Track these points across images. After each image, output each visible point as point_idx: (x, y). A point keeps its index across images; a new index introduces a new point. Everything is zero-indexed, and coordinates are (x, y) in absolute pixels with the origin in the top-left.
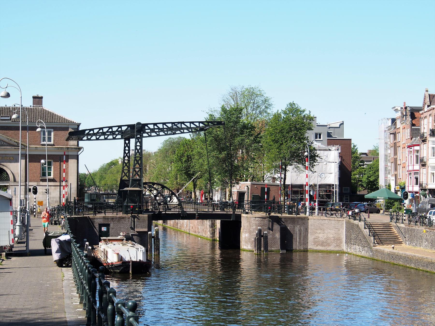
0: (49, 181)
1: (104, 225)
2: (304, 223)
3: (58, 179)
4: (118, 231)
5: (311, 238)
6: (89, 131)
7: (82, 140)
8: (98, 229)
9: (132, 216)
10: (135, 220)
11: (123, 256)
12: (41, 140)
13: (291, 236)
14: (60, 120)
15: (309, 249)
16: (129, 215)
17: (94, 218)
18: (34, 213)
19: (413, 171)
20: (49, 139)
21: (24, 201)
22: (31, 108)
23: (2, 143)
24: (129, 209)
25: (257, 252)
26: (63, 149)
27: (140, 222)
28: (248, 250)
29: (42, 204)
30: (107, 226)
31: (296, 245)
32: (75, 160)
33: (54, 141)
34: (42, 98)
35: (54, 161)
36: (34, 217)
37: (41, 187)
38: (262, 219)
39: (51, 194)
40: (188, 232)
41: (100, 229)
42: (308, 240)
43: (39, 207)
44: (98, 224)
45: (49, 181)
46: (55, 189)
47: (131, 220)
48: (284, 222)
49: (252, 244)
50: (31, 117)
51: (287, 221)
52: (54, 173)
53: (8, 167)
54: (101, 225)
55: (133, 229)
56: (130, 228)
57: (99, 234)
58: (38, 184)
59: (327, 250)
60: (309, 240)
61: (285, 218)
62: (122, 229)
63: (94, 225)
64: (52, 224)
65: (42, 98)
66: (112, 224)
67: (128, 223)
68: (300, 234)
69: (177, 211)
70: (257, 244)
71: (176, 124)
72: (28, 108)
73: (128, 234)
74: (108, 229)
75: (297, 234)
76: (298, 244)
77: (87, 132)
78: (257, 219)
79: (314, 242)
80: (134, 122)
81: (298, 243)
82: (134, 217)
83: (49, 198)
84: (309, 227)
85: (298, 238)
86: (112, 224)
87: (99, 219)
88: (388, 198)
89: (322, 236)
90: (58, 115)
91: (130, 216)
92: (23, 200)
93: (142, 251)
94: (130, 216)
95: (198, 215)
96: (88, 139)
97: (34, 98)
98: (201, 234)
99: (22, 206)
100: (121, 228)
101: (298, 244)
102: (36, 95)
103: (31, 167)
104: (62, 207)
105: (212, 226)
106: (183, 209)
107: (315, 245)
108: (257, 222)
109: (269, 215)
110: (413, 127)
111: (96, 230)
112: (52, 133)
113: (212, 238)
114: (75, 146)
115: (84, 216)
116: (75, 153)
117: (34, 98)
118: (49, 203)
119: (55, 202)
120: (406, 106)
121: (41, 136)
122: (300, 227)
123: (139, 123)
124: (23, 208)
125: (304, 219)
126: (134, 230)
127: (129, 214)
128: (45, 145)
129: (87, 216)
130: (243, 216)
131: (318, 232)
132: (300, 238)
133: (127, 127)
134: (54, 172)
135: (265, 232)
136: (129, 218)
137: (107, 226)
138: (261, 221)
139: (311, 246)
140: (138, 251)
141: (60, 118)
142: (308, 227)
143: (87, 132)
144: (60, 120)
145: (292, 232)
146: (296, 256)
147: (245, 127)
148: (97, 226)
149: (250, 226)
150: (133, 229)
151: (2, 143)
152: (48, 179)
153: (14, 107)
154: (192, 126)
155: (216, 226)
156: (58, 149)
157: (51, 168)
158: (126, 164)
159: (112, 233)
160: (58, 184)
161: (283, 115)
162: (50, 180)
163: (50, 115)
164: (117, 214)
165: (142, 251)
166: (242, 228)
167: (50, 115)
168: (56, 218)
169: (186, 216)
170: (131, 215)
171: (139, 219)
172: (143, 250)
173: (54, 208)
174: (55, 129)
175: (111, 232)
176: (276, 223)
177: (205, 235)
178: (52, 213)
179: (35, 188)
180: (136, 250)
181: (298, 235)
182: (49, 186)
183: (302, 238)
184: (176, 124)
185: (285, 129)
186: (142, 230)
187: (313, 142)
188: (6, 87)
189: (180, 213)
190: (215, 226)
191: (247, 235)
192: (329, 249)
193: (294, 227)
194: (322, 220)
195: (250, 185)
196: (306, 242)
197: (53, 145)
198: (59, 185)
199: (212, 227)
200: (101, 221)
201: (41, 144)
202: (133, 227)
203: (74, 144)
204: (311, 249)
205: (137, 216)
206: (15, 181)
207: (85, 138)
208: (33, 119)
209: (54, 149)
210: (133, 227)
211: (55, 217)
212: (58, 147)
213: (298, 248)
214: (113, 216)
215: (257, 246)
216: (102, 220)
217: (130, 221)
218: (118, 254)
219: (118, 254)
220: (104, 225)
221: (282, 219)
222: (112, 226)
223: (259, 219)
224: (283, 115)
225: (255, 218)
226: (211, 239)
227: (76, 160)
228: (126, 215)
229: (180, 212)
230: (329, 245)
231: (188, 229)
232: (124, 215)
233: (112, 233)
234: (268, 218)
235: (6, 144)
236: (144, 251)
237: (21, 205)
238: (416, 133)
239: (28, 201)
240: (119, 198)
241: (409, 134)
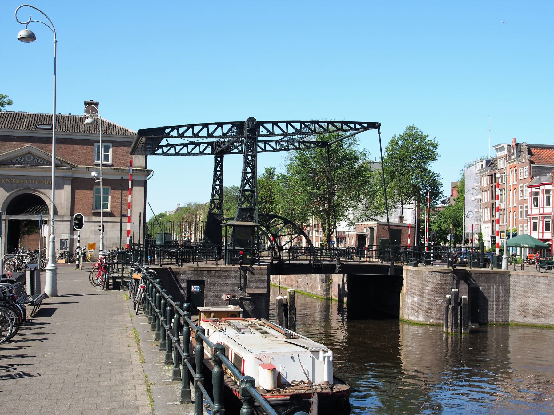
0: (103, 216)
1: (196, 283)
2: (503, 281)
3: (118, 213)
4: (219, 293)
5: (513, 304)
6: (170, 129)
7: (154, 154)
8: (185, 288)
9: (242, 268)
10: (247, 274)
11: (283, 374)
12: (94, 158)
13: (485, 301)
14: (122, 132)
15: (511, 321)
16: (236, 266)
17: (180, 270)
18: (77, 262)
19: (540, 214)
20: (106, 158)
21: (66, 242)
22: (82, 117)
23: (39, 161)
24: (236, 256)
25: (452, 331)
26: (125, 171)
27: (255, 278)
28: (418, 322)
29: (94, 248)
30: (201, 283)
31: (493, 317)
32: (141, 187)
33: (113, 160)
34: (97, 104)
35: (112, 189)
36: (76, 267)
37: (94, 223)
38: (442, 274)
39: (108, 233)
40: (278, 285)
41: (189, 289)
42: (509, 307)
43: (90, 251)
44: (185, 281)
45: (103, 216)
46: (113, 227)
47: (241, 274)
48: (475, 279)
49: (426, 314)
50: (81, 127)
51: (479, 278)
52: (112, 205)
53: (47, 195)
54: (190, 283)
55: (242, 289)
56: (238, 287)
57: (187, 297)
58: (89, 219)
59: (543, 325)
60: (510, 307)
61: (476, 273)
62: (225, 290)
63: (178, 283)
64: (108, 288)
65: (97, 104)
66: (209, 281)
67: (234, 280)
68: (498, 298)
69: (306, 260)
70: (452, 316)
71: (307, 124)
72: (78, 117)
73: (235, 297)
74: (202, 289)
75: (493, 298)
76: (494, 314)
77: (167, 131)
78: (434, 274)
79: (519, 311)
80: (243, 118)
81: (494, 313)
82: (245, 270)
83: (103, 236)
84: (511, 287)
85: (494, 304)
86: (209, 281)
87: (187, 272)
88: (536, 245)
89: (532, 302)
90: (119, 126)
91: (239, 268)
92: (65, 240)
93: (326, 359)
94: (239, 268)
95: (339, 267)
96: (165, 154)
97: (86, 103)
98: (303, 289)
99: (64, 250)
100: (223, 287)
101: (494, 314)
102: (89, 100)
103: (79, 195)
104: (125, 252)
105: (326, 280)
106: (317, 257)
107: (522, 316)
108: (435, 280)
109: (453, 269)
110: (532, 165)
111: (183, 290)
112: (111, 150)
113: (326, 296)
114: (141, 167)
115: (163, 266)
116: (141, 178)
117: (86, 103)
118: (103, 244)
119: (113, 245)
120: (517, 143)
121: (94, 153)
122: (498, 287)
123: (251, 119)
124: (65, 253)
125: (504, 275)
126: (244, 291)
127: (238, 264)
128: (99, 165)
129: (168, 267)
130: (407, 270)
131: (527, 295)
132: (497, 305)
133: (231, 126)
134: (112, 202)
135: (463, 297)
136: (236, 271)
137: (201, 283)
138: (441, 277)
139: (514, 317)
140: (316, 359)
141: (121, 129)
142: (509, 287)
143: (167, 131)
144: (122, 132)
145: (486, 295)
146: (493, 334)
147: (346, 157)
148: (184, 285)
149: (423, 286)
150: (242, 289)
151: (39, 161)
152: (103, 213)
153: (58, 115)
154: (332, 128)
155: (332, 279)
156: (119, 172)
157: (108, 197)
158: (217, 191)
159: (209, 296)
160: (118, 219)
161: (400, 143)
162: (106, 214)
163: (107, 126)
164: (217, 264)
165: (326, 359)
166: (404, 289)
167: (107, 126)
168: (115, 271)
169: (321, 268)
170: (241, 265)
171: (253, 274)
172: (329, 357)
173: (113, 253)
174: (115, 144)
175: (206, 294)
176: (463, 281)
177: (312, 291)
178: (109, 264)
179: (79, 217)
180: (312, 355)
181: (494, 300)
182: (103, 222)
183: (500, 305)
184: (307, 124)
185: (407, 157)
186: (258, 290)
187: (439, 175)
188: (28, 23)
189: (312, 263)
190: (329, 280)
191: (416, 299)
192: (546, 323)
193: (489, 287)
194: (534, 276)
195: (376, 225)
196: (506, 312)
197: (112, 166)
198: (119, 221)
199: (326, 282)
200: (191, 276)
201: (94, 163)
202: (242, 285)
203: (140, 165)
204: (514, 321)
205: (251, 269)
206: (56, 213)
207: (160, 151)
208: (83, 130)
209: (112, 171)
210: (242, 285)
211: (113, 269)
212: (119, 168)
213: (494, 320)
214: (211, 268)
215: (452, 320)
216: (192, 274)
217: (239, 276)
218: (274, 370)
219: (274, 370)
220: (196, 283)
221: (472, 274)
222: (209, 284)
223: (438, 274)
224: (400, 143)
225: (430, 273)
226: (325, 297)
227: (143, 188)
228: (231, 266)
229: (312, 262)
230: (545, 316)
231: (277, 281)
232: (227, 266)
233: (209, 296)
234: (452, 272)
235: (45, 162)
236: (331, 359)
237: (62, 248)
238: (535, 172)
239: (53, 235)
240: (205, 240)
241: (527, 173)
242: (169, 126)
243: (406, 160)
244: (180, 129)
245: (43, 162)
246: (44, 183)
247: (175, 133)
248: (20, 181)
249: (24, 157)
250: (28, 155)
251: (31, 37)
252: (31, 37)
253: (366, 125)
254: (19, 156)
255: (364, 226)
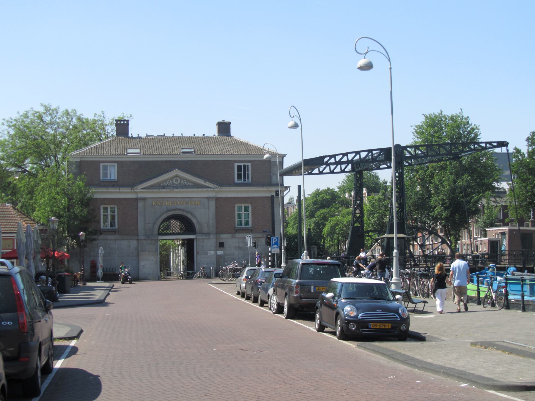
23: (186, 183)
77: (326, 159)
143: (326, 159)
195: (507, 230)
235: (189, 183)
242: (327, 155)
243: (11, 124)
244: (337, 157)
245: (189, 183)
246: (191, 204)
247: (332, 160)
248: (169, 203)
249: (172, 181)
250: (175, 178)
251: (368, 67)
252: (368, 67)
253: (495, 144)
254: (167, 180)
255: (496, 232)
